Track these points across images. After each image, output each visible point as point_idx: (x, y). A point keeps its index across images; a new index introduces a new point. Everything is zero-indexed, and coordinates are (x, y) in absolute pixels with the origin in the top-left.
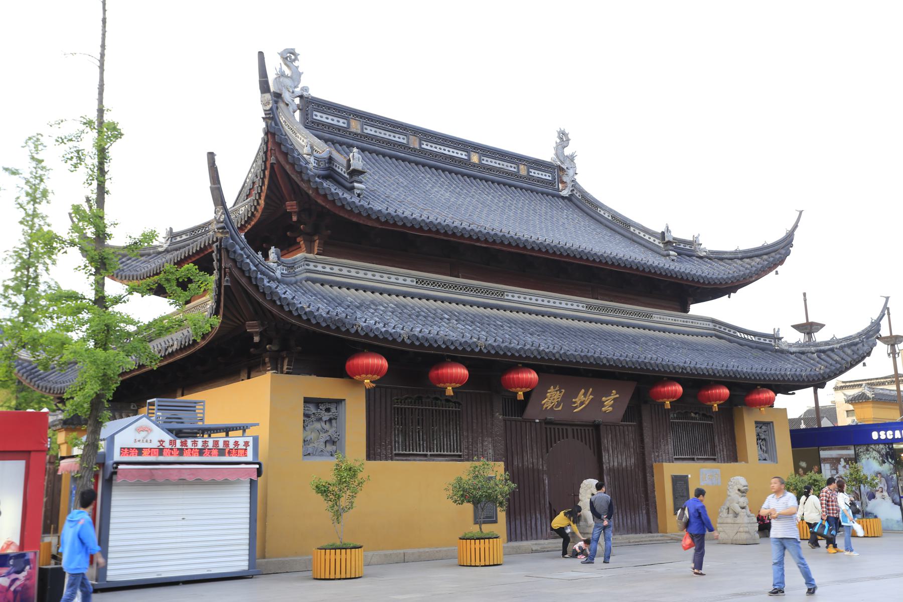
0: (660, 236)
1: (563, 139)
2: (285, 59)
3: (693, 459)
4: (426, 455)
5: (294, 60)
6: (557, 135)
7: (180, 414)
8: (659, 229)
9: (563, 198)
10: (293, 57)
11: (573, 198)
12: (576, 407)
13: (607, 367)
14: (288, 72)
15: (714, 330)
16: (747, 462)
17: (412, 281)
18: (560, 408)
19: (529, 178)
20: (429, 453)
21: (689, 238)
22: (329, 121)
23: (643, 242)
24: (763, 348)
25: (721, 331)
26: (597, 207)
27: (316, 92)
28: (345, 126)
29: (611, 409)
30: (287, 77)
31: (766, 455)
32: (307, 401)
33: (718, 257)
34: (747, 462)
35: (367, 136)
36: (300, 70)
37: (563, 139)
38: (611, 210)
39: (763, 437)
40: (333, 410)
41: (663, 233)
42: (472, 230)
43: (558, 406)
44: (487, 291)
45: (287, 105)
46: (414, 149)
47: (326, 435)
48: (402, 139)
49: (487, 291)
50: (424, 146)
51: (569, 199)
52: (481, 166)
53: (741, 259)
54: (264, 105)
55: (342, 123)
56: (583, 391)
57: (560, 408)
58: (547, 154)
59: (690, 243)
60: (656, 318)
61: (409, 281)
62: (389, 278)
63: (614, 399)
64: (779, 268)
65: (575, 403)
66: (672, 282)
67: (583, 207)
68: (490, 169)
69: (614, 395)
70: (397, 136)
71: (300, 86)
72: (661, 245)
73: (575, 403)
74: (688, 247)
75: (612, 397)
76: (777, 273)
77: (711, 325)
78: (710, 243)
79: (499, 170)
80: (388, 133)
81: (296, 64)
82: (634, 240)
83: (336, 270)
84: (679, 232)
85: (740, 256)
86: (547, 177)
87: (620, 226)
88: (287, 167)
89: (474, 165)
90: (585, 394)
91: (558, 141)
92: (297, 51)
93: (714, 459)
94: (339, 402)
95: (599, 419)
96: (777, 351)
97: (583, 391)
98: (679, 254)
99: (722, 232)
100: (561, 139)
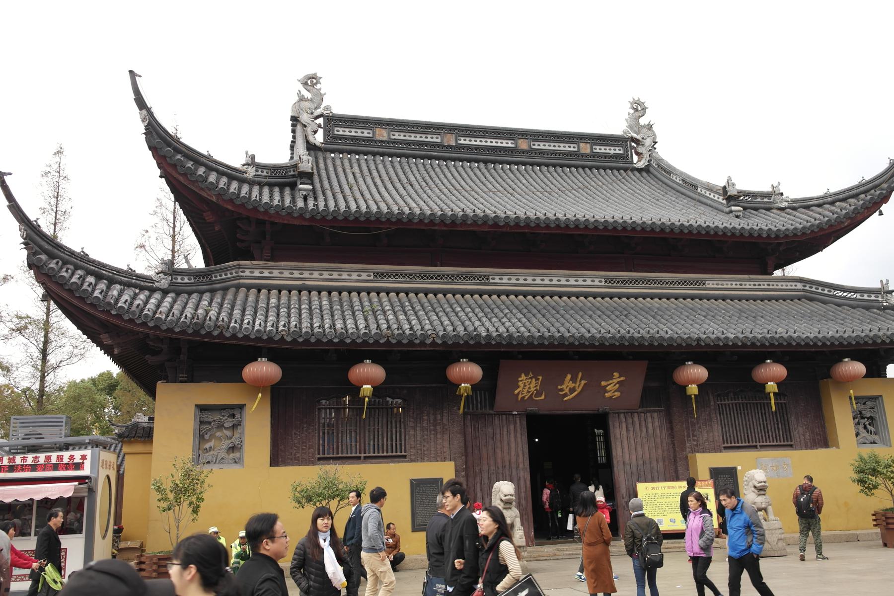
0: (721, 192)
1: (639, 109)
2: (305, 84)
3: (756, 447)
4: (359, 458)
5: (316, 84)
6: (629, 105)
7: (39, 430)
8: (722, 183)
9: (640, 170)
10: (315, 81)
11: (651, 169)
12: (566, 395)
13: (869, 345)
14: (308, 95)
15: (804, 291)
16: (838, 447)
17: (600, 281)
18: (543, 397)
19: (594, 155)
20: (758, 444)
21: (766, 188)
22: (353, 134)
23: (709, 202)
24: (867, 307)
25: (816, 293)
26: (670, 173)
27: (339, 109)
28: (370, 135)
29: (617, 394)
30: (307, 100)
31: (876, 437)
32: (202, 408)
33: (805, 205)
34: (838, 447)
35: (395, 142)
36: (322, 92)
37: (639, 109)
38: (682, 173)
39: (868, 415)
40: (238, 416)
41: (725, 187)
42: (725, 227)
43: (539, 394)
44: (636, 281)
45: (305, 126)
46: (586, 155)
47: (229, 442)
48: (436, 139)
49: (636, 281)
50: (462, 142)
51: (647, 170)
52: (531, 152)
53: (832, 203)
54: (143, 121)
55: (366, 133)
56: (569, 376)
57: (543, 397)
58: (617, 127)
59: (768, 195)
60: (710, 284)
61: (364, 276)
62: (252, 272)
63: (618, 382)
64: (884, 208)
65: (562, 390)
66: (756, 243)
67: (659, 176)
68: (541, 152)
69: (617, 377)
70: (429, 136)
71: (322, 107)
72: (724, 202)
73: (562, 390)
74: (766, 200)
75: (615, 381)
76: (881, 214)
77: (800, 286)
78: (793, 191)
79: (554, 153)
80: (418, 135)
81: (318, 86)
82: (702, 202)
83: (257, 273)
84: (745, 183)
85: (830, 199)
86: (618, 151)
87: (689, 188)
88: (181, 179)
89: (523, 151)
90: (574, 379)
91: (632, 111)
92: (318, 75)
93: (791, 446)
94: (241, 407)
95: (603, 407)
96: (886, 308)
97: (569, 376)
98: (745, 209)
99: (808, 174)
100: (636, 110)
